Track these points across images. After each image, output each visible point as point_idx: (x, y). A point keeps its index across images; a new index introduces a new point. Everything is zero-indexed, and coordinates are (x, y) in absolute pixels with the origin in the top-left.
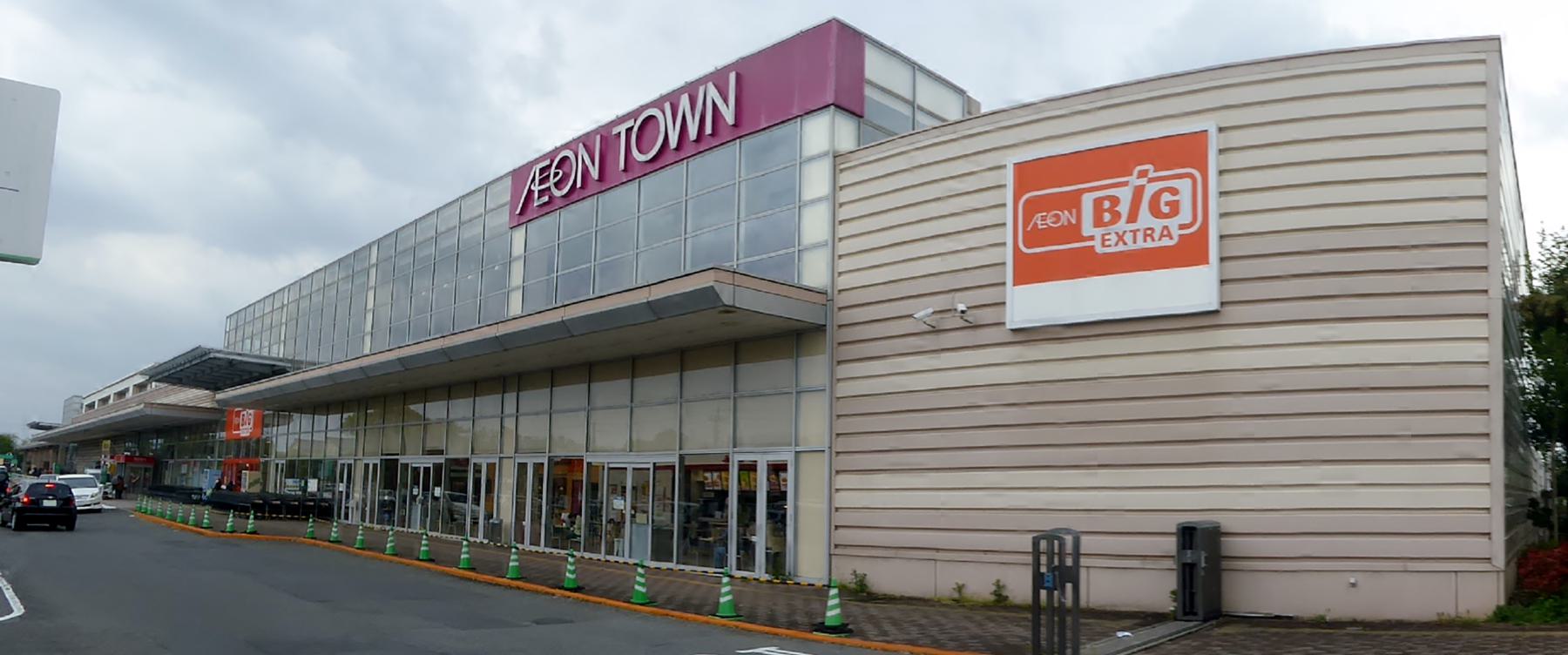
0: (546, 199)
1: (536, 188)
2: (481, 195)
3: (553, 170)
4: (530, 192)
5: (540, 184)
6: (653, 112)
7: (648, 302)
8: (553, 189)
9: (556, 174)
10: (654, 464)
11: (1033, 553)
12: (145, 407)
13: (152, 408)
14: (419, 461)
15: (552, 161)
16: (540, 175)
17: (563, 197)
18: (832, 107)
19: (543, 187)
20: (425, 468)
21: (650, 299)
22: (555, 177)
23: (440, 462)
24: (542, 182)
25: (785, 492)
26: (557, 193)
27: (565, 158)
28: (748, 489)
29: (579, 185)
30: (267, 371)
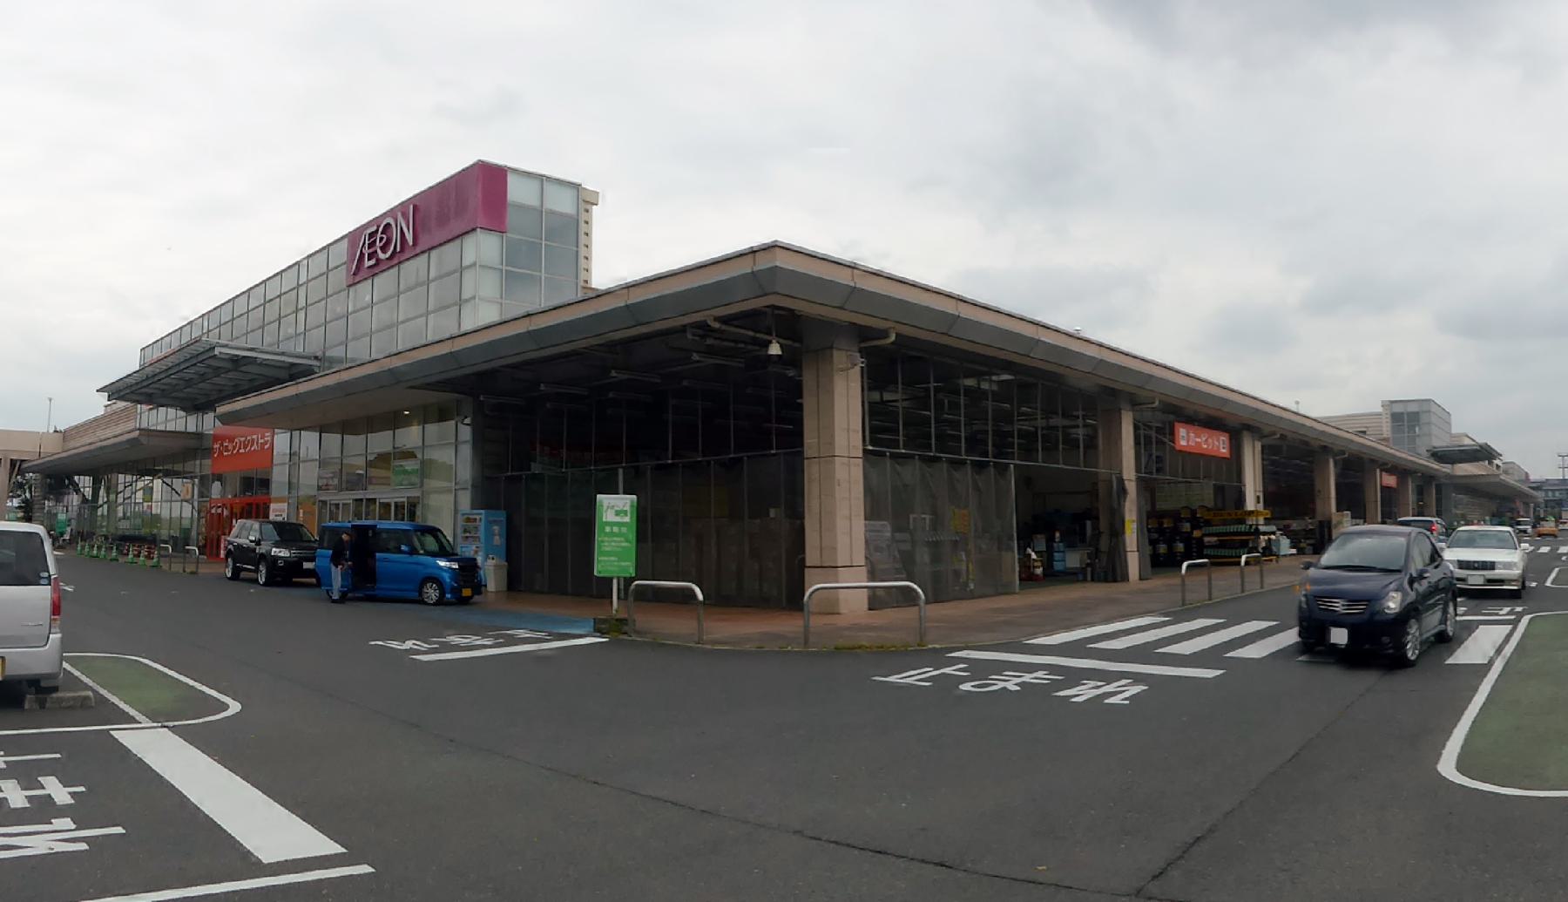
0: (372, 262)
1: (366, 251)
2: (244, 298)
3: (379, 235)
4: (362, 254)
5: (369, 248)
6: (390, 220)
7: (627, 306)
8: (379, 251)
9: (381, 239)
10: (408, 498)
11: (805, 567)
12: (140, 434)
13: (149, 436)
14: (389, 496)
15: (378, 227)
16: (369, 240)
17: (387, 259)
18: (478, 230)
19: (371, 250)
20: (396, 503)
21: (629, 302)
22: (380, 242)
23: (402, 500)
24: (370, 246)
25: (872, 513)
26: (382, 256)
27: (388, 225)
28: (294, 521)
29: (398, 250)
30: (283, 374)
